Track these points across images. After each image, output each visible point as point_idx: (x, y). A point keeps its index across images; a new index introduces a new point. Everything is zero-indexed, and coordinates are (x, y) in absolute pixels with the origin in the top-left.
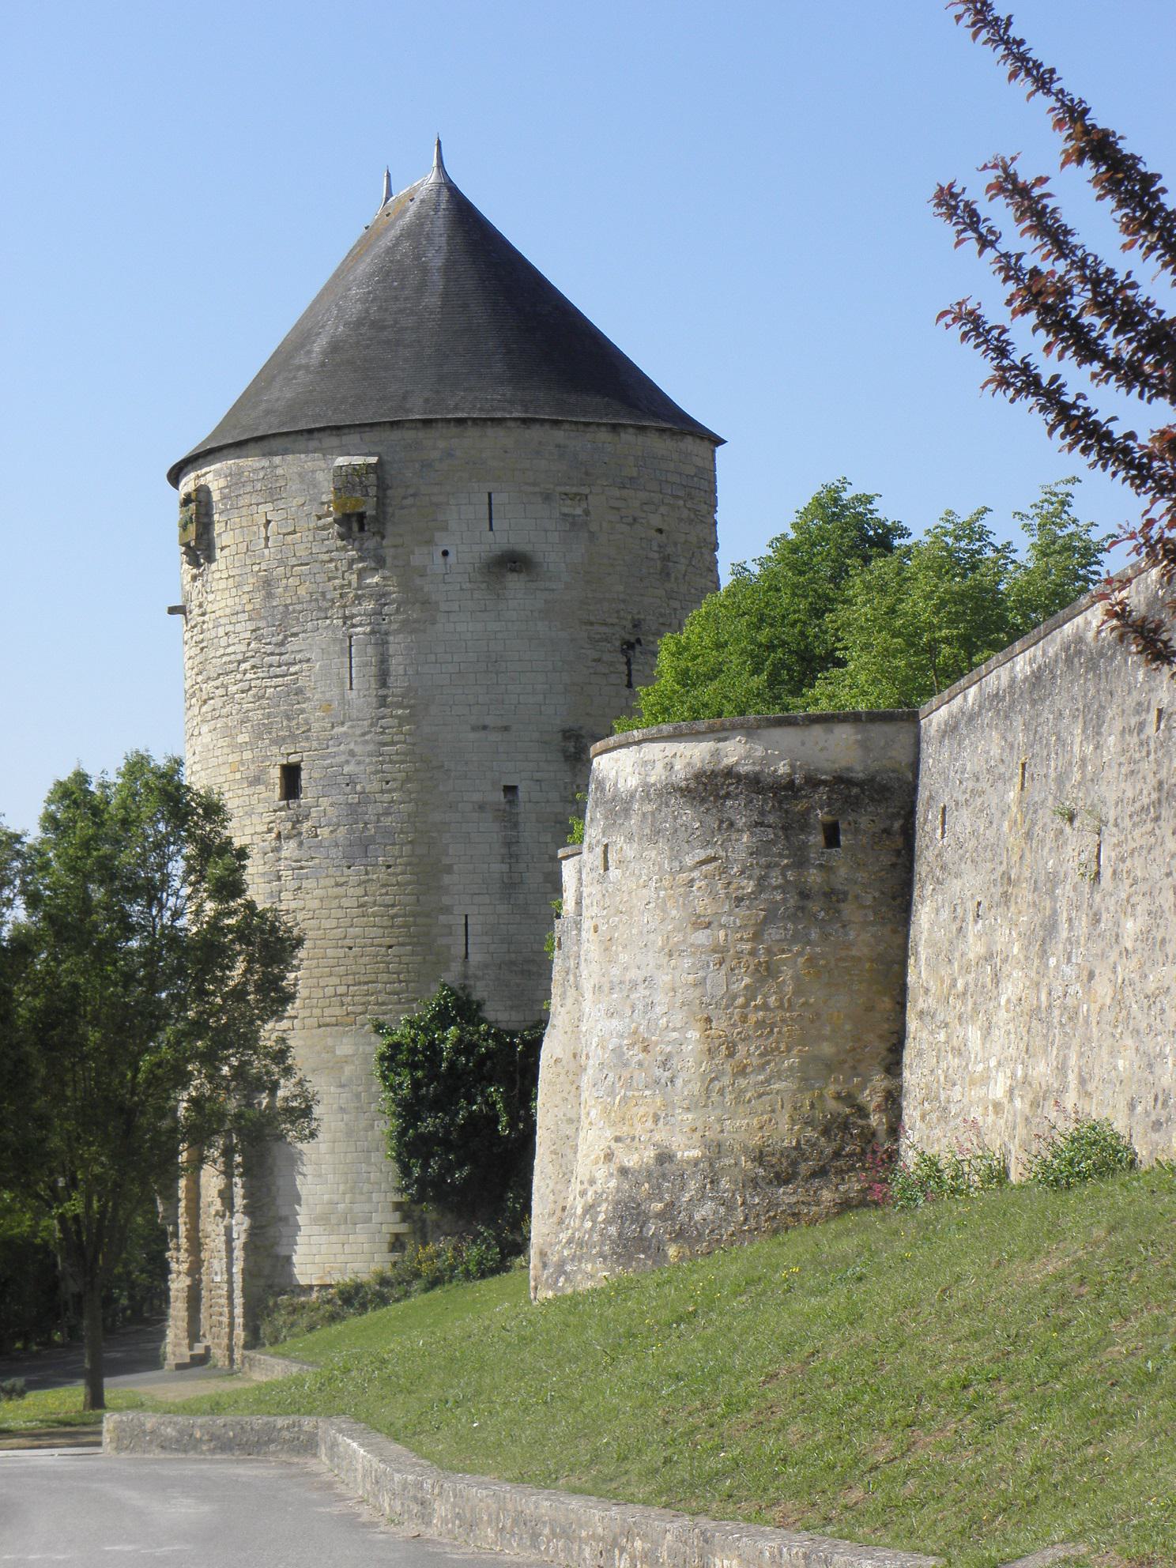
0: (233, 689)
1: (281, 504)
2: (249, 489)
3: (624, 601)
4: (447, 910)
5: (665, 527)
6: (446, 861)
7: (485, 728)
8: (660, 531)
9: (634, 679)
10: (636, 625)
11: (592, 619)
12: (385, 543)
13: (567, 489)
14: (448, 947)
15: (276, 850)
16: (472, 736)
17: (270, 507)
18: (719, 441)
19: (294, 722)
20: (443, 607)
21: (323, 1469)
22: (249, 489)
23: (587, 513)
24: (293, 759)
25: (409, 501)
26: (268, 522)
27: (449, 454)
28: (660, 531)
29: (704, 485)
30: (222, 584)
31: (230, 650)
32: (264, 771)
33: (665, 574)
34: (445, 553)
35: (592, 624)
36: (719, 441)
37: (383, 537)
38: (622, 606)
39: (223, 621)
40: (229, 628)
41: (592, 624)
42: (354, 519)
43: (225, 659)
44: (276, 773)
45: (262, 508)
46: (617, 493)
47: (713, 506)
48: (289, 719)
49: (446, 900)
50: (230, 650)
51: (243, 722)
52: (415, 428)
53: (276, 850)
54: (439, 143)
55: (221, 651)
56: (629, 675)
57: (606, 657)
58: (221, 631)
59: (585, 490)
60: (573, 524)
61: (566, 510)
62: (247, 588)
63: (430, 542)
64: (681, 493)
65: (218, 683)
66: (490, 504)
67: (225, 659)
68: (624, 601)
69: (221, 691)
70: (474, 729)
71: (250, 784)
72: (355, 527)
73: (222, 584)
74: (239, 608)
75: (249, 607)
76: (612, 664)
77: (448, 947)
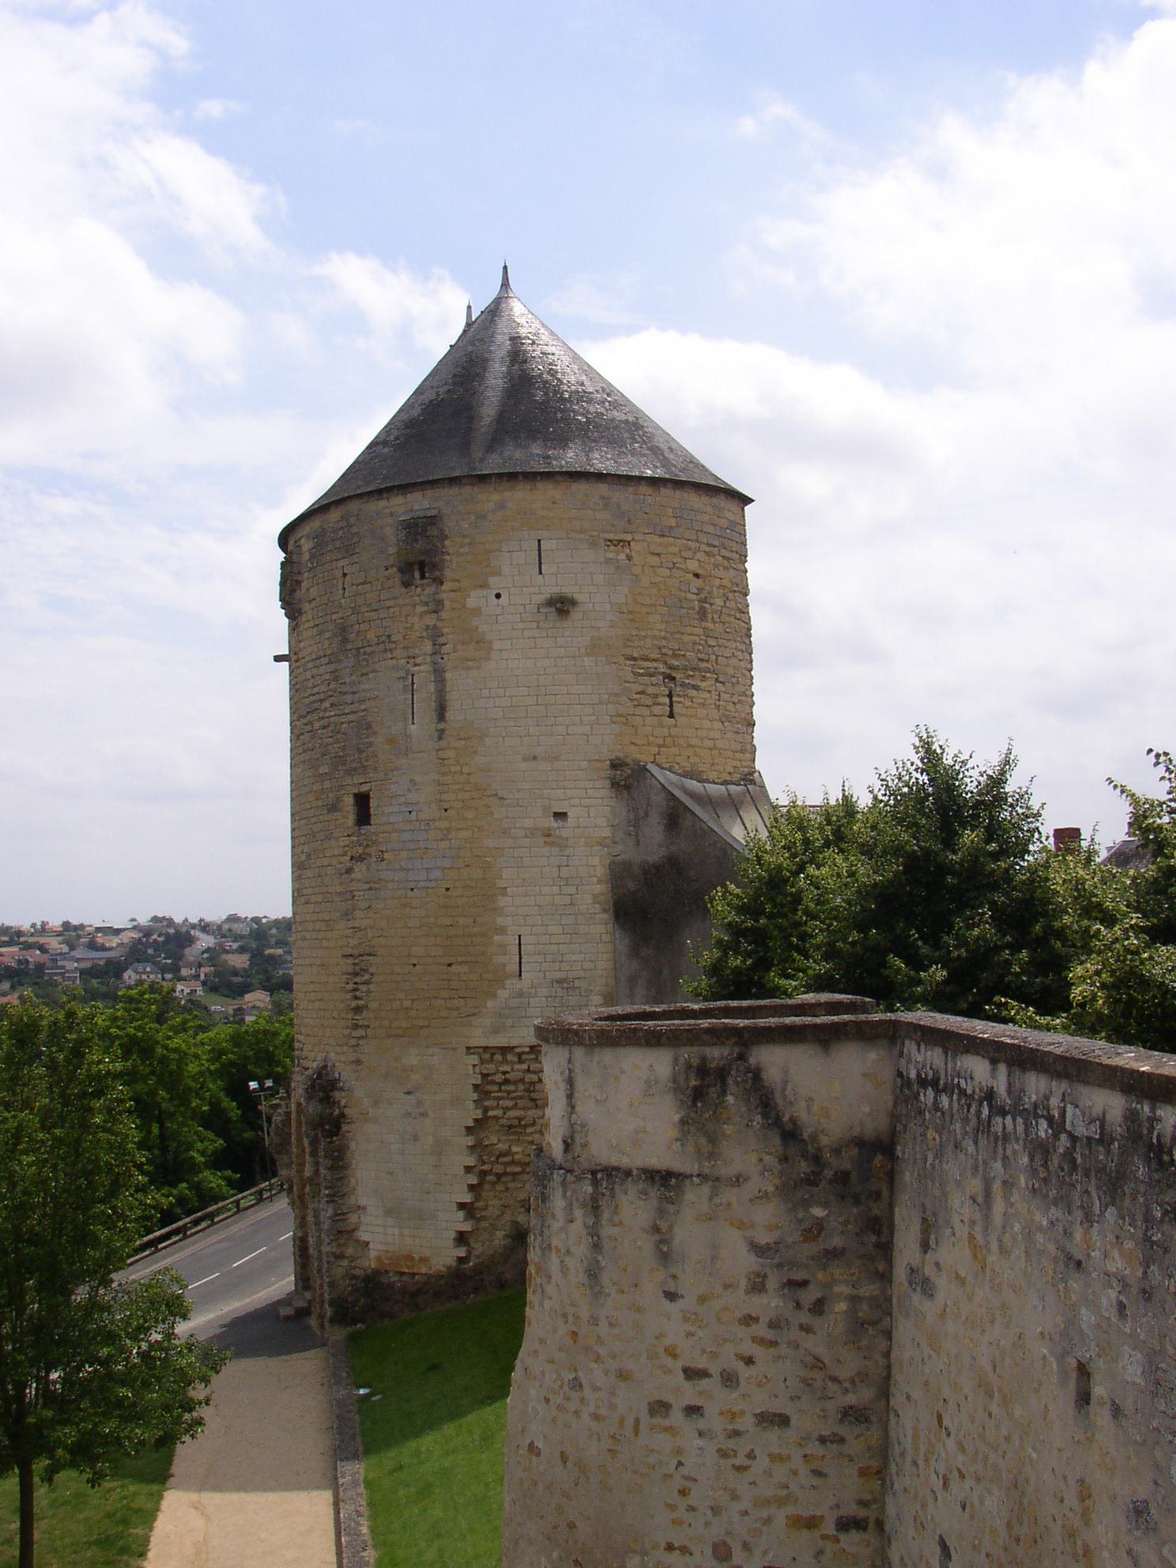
0: (317, 725)
1: (355, 558)
2: (330, 547)
3: (665, 638)
4: (502, 930)
5: (700, 572)
6: (501, 883)
7: (535, 758)
8: (697, 576)
9: (675, 709)
10: (722, 1413)
11: (636, 655)
12: (444, 587)
13: (611, 536)
14: (504, 965)
15: (349, 871)
16: (524, 765)
17: (345, 562)
18: (747, 500)
19: (364, 755)
20: (497, 645)
21: (481, 1249)
22: (330, 547)
23: (629, 558)
24: (364, 788)
25: (466, 549)
26: (345, 575)
27: (501, 506)
28: (697, 576)
29: (736, 537)
30: (309, 633)
31: (316, 690)
32: (339, 799)
33: (703, 614)
34: (498, 596)
35: (635, 659)
36: (747, 500)
37: (442, 583)
38: (664, 643)
39: (310, 665)
40: (315, 671)
41: (635, 659)
42: (416, 567)
43: (312, 698)
44: (349, 800)
45: (340, 563)
46: (658, 539)
47: (743, 557)
48: (360, 751)
49: (500, 921)
50: (316, 690)
51: (323, 755)
52: (472, 485)
53: (349, 871)
54: (505, 268)
55: (309, 692)
56: (671, 706)
57: (651, 690)
58: (308, 675)
59: (629, 537)
60: (618, 568)
61: (611, 555)
62: (328, 635)
63: (484, 586)
64: (716, 543)
65: (305, 721)
66: (539, 550)
67: (312, 698)
68: (665, 638)
69: (309, 728)
70: (525, 760)
71: (329, 811)
72: (417, 574)
73: (309, 633)
74: (321, 653)
75: (329, 652)
76: (656, 696)
77: (504, 965)
